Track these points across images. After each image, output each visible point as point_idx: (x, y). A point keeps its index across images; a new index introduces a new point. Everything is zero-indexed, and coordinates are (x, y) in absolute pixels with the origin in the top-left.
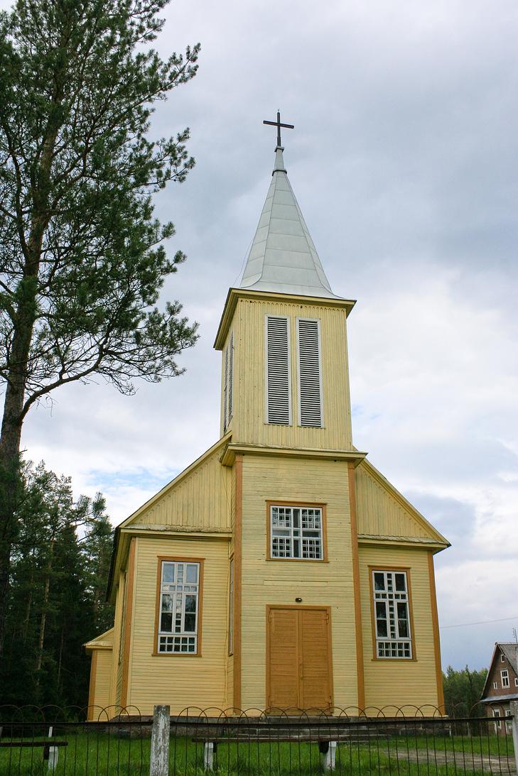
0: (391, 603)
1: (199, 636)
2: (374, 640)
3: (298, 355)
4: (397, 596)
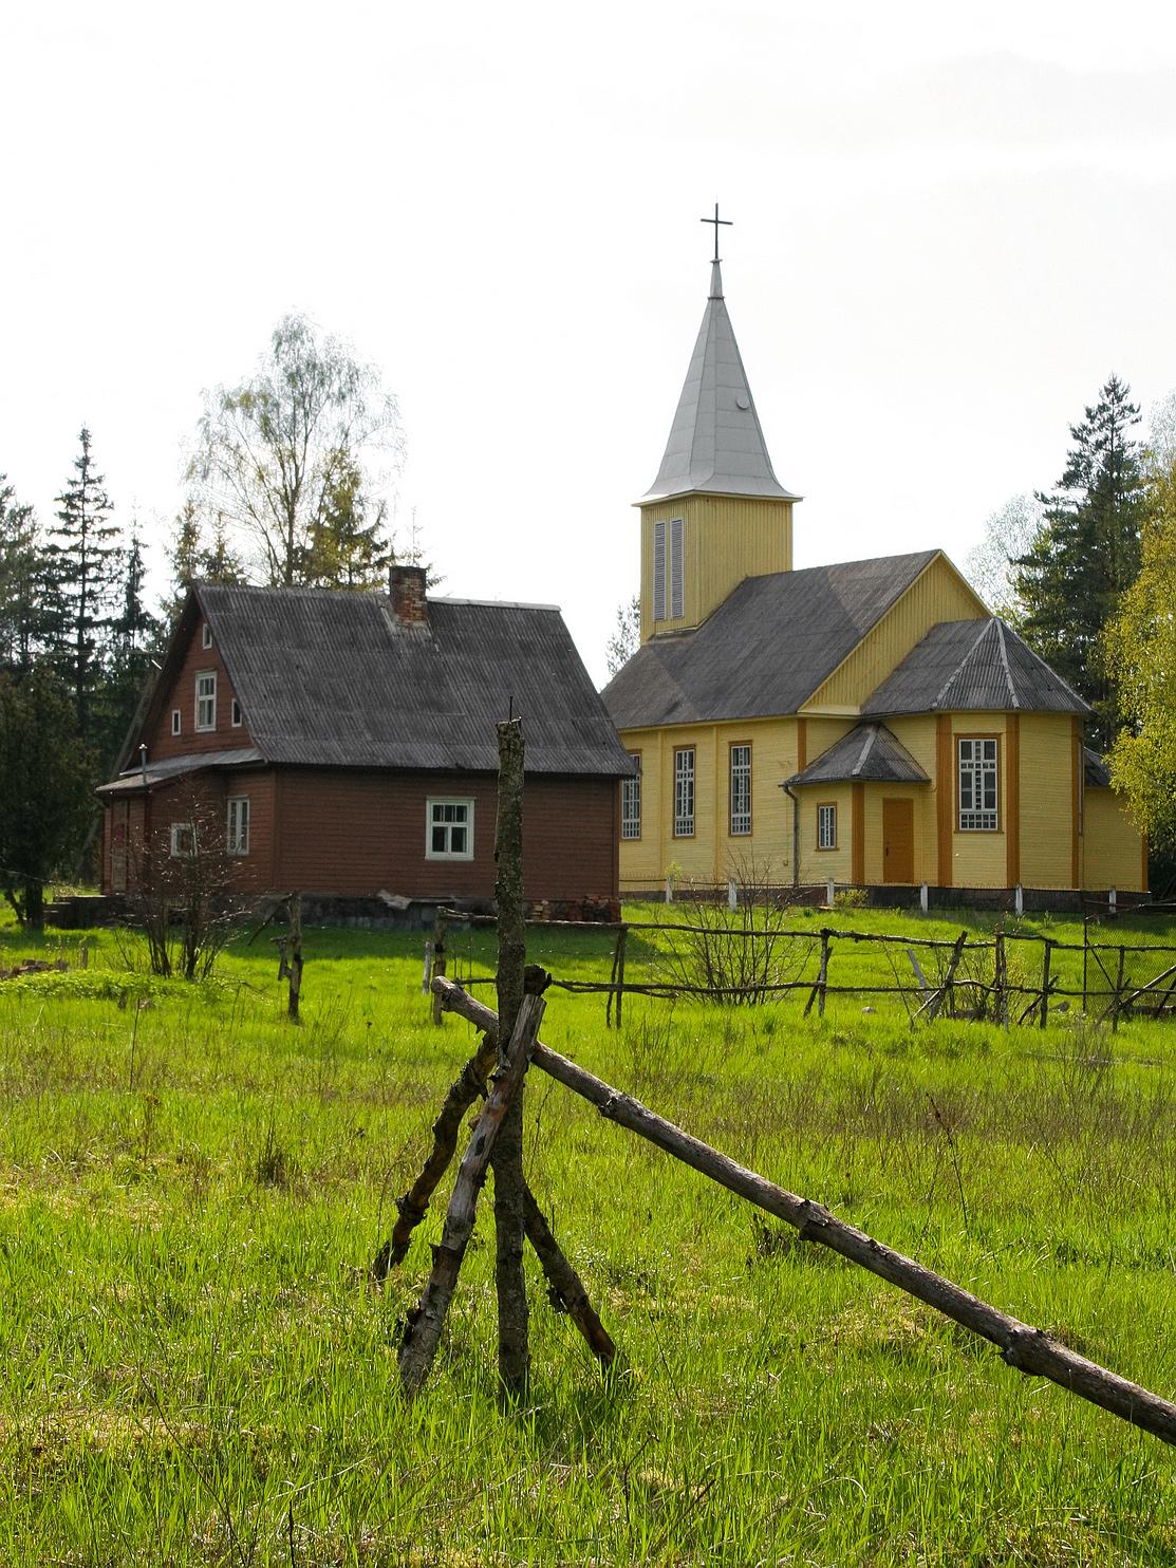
0: (978, 773)
1: (674, 779)
2: (958, 813)
4: (985, 766)
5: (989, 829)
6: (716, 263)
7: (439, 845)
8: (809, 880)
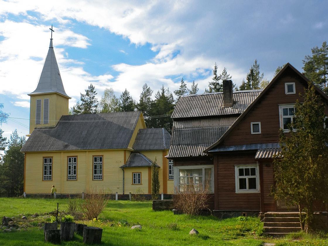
0: (72, 166)
1: (77, 175)
5: (97, 179)
6: (51, 39)
7: (242, 185)
8: (126, 193)
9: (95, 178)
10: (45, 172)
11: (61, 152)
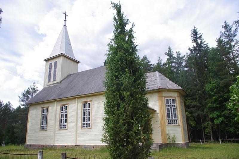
0: (171, 108)
3: (90, 145)
9: (61, 128)
10: (84, 118)
11: (75, 98)
